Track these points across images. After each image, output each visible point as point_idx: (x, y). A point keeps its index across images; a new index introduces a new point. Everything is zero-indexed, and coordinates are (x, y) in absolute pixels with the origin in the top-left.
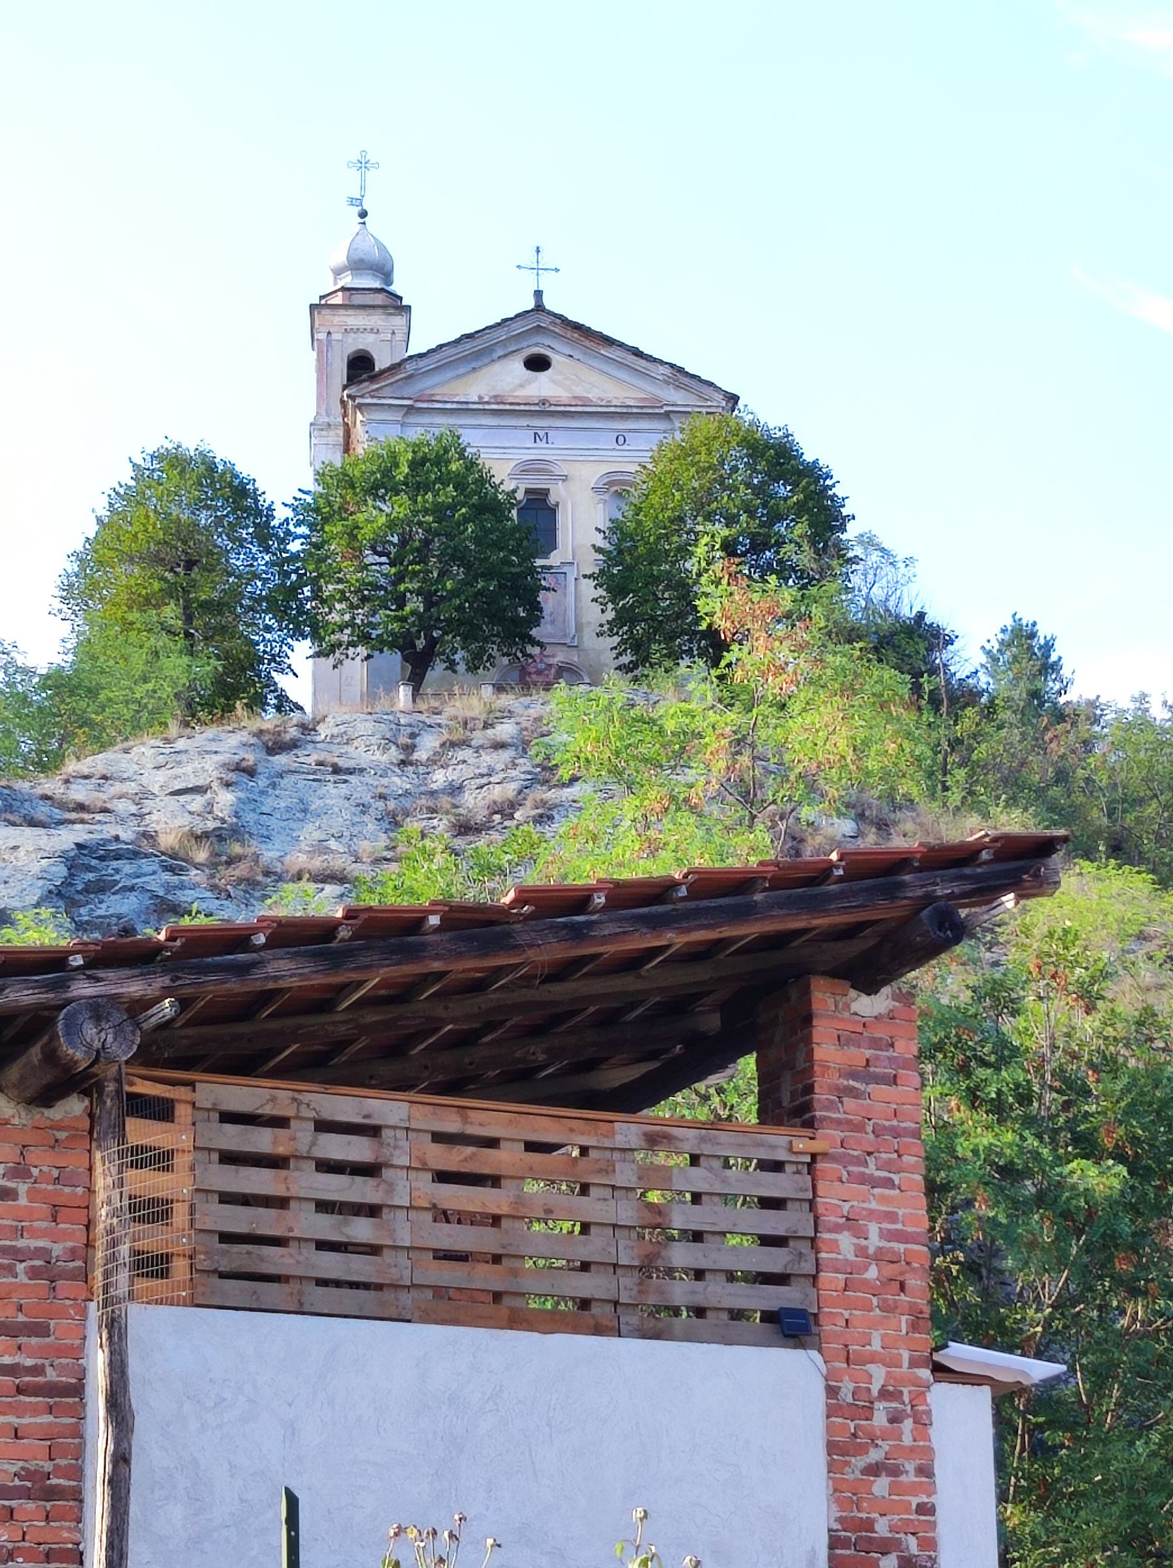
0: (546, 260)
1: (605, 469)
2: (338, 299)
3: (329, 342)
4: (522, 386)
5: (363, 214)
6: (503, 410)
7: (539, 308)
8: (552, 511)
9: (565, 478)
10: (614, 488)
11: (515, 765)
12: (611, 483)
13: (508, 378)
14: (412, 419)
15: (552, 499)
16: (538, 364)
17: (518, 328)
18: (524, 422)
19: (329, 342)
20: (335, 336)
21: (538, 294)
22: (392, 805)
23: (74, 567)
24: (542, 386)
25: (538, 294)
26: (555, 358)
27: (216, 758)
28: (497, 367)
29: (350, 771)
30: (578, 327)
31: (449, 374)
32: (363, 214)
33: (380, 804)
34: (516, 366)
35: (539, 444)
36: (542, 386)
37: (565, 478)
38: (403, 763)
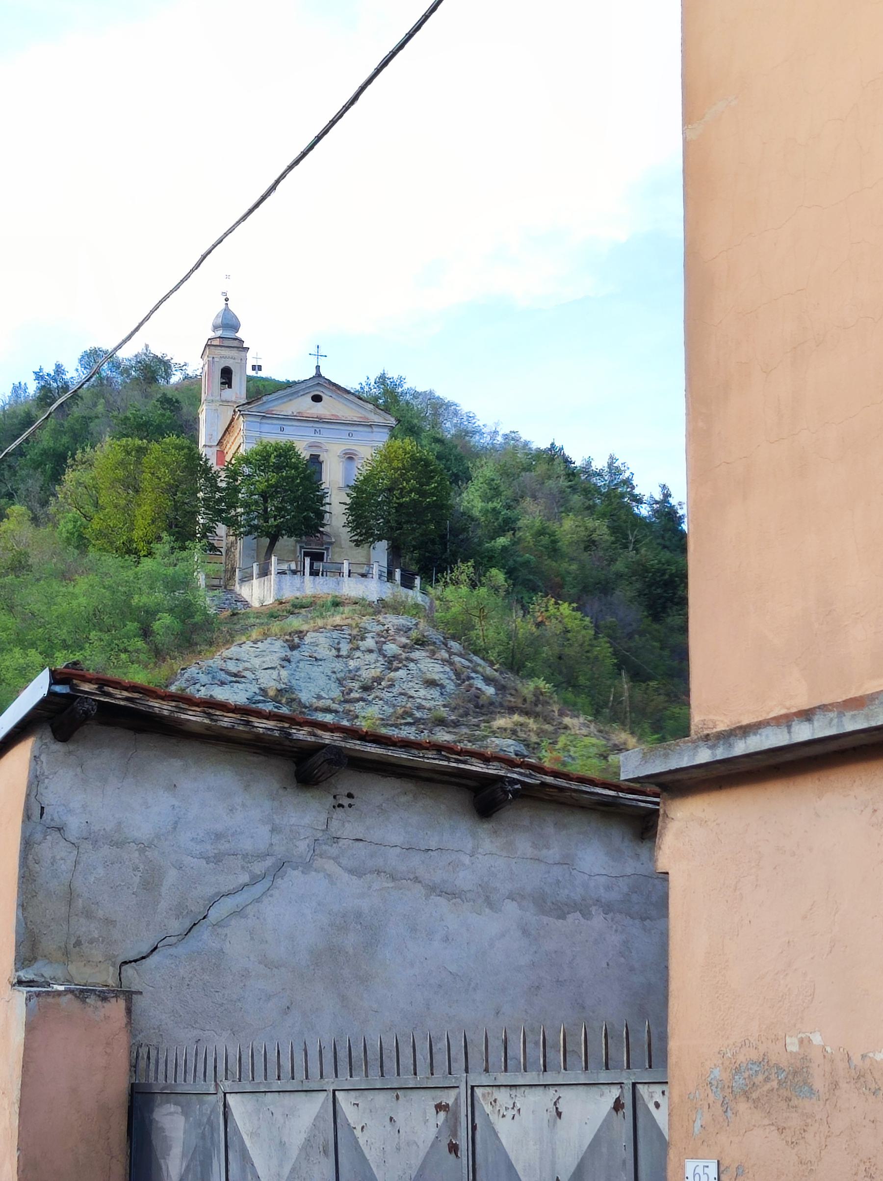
0: (321, 352)
1: (344, 447)
2: (216, 342)
3: (213, 362)
4: (310, 408)
5: (227, 300)
6: (301, 419)
7: (318, 375)
8: (321, 463)
9: (327, 451)
10: (360, 470)
11: (378, 661)
12: (346, 454)
13: (304, 405)
14: (264, 421)
15: (321, 459)
16: (317, 399)
17: (311, 384)
18: (311, 425)
19: (213, 362)
20: (216, 359)
21: (318, 367)
22: (339, 676)
23: (33, 388)
24: (318, 409)
25: (318, 367)
26: (324, 397)
27: (277, 655)
28: (300, 399)
29: (321, 660)
30: (335, 385)
31: (280, 401)
32: (227, 300)
33: (334, 676)
34: (308, 398)
35: (317, 435)
36: (318, 409)
37: (327, 451)
38: (338, 656)
